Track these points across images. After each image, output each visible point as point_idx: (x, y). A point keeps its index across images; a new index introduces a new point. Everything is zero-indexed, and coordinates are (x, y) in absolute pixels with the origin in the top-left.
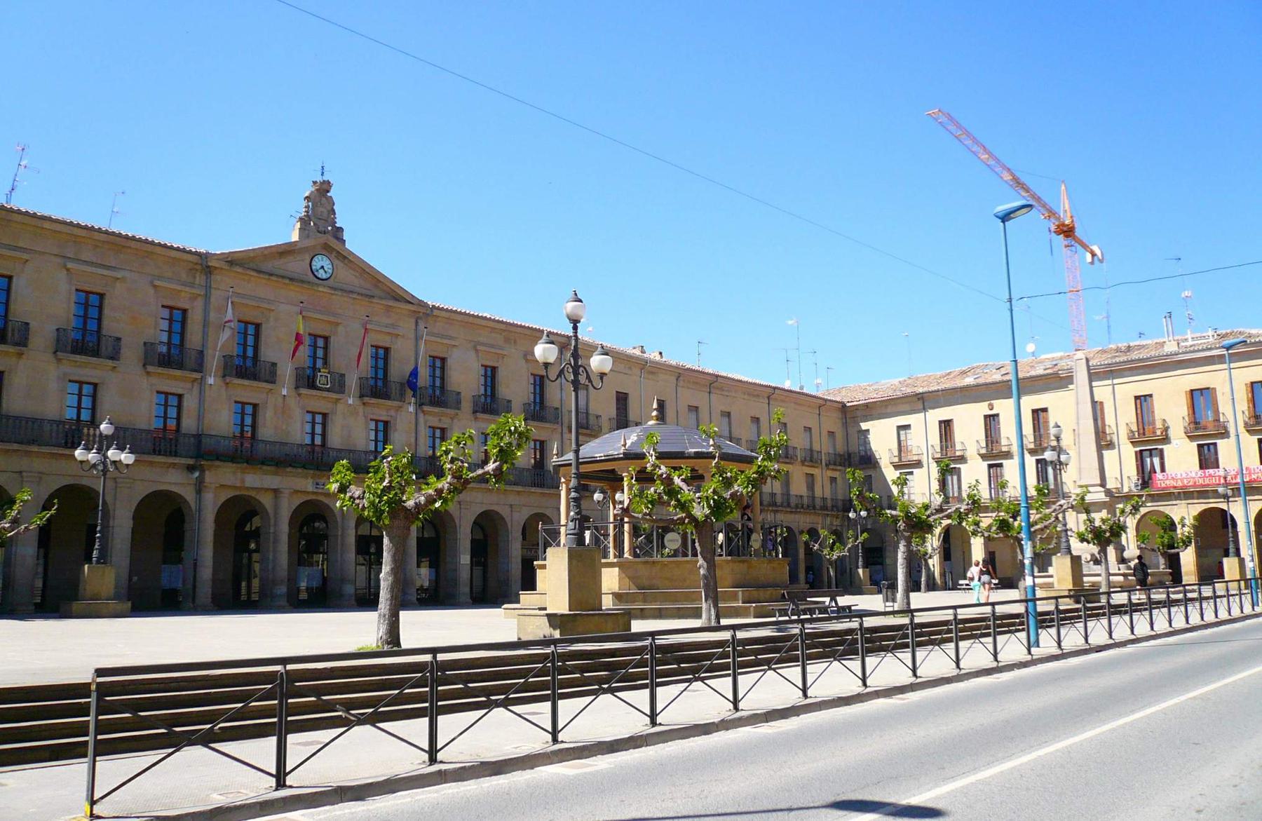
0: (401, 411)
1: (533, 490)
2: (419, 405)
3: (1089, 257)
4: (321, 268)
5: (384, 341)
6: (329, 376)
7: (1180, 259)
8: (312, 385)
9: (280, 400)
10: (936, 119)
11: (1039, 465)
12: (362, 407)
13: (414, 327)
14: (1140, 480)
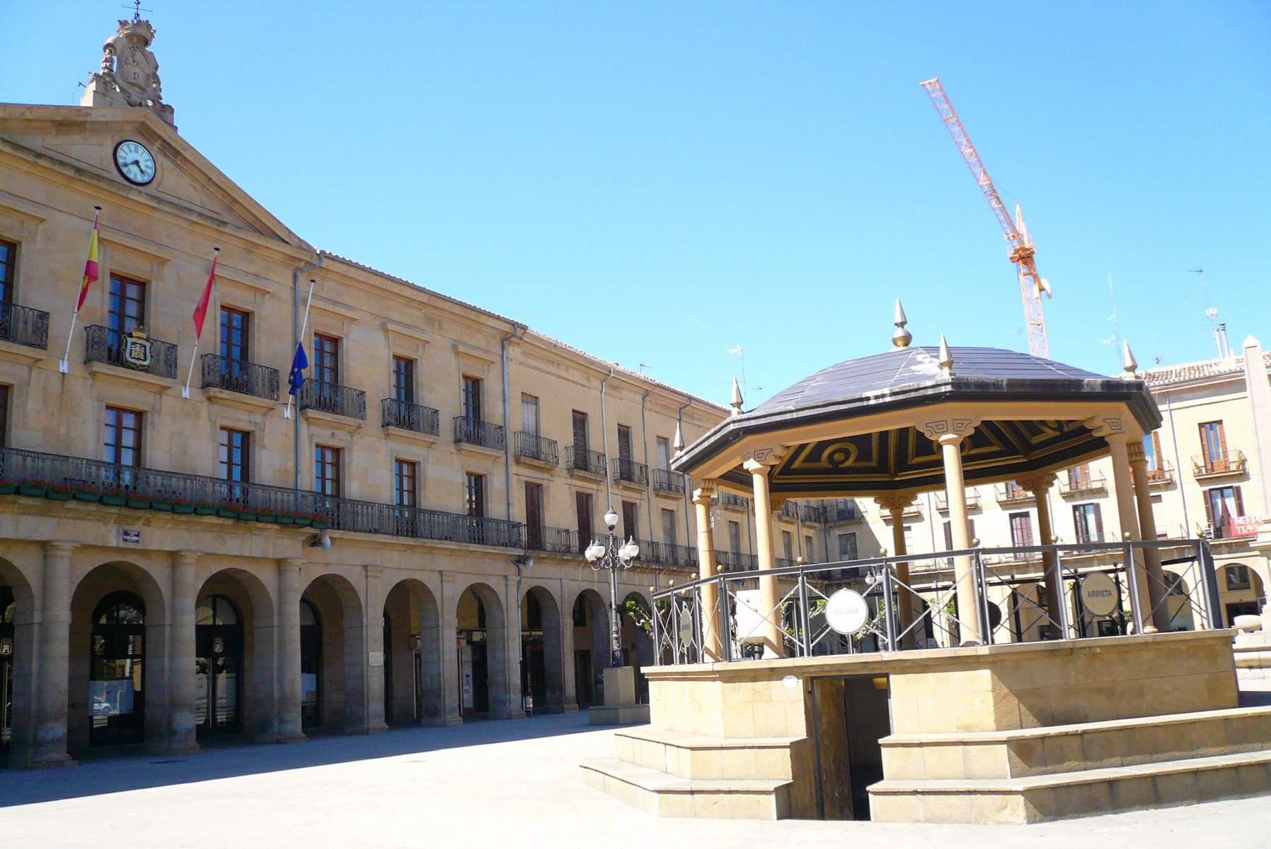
0: (272, 416)
1: (473, 547)
2: (301, 409)
3: (1036, 288)
4: (133, 163)
5: (242, 300)
6: (148, 345)
7: (1201, 271)
8: (116, 358)
9: (55, 381)
10: (929, 93)
11: (1077, 513)
12: (206, 404)
13: (290, 283)
14: (1212, 527)
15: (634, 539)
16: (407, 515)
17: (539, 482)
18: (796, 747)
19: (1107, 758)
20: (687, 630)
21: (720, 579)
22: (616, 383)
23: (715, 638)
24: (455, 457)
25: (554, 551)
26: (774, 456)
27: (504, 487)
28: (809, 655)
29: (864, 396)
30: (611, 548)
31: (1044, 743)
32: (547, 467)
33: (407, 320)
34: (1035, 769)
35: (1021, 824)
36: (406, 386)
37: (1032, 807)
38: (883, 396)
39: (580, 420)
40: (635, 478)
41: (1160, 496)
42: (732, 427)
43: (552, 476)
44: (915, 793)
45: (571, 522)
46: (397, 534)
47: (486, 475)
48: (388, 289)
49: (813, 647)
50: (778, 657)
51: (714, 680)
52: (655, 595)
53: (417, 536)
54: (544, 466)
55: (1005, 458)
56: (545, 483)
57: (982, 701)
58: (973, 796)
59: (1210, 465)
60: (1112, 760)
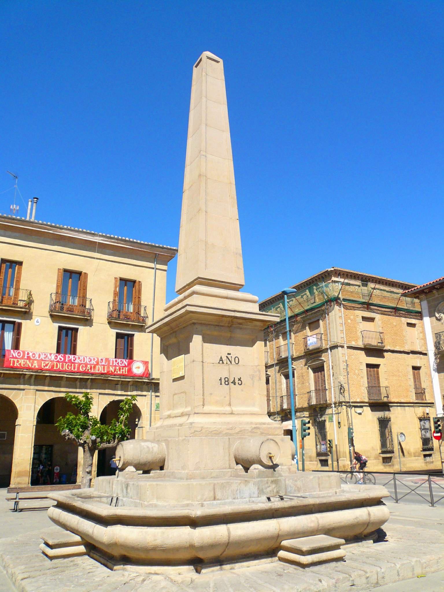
41: (133, 335)
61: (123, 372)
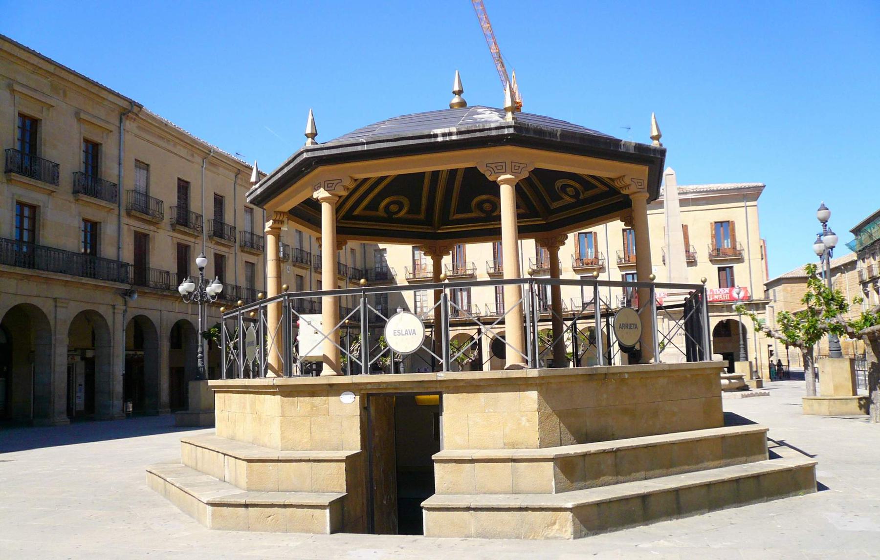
1: (85, 280)
7: (629, 128)
15: (219, 279)
16: (25, 249)
17: (147, 232)
18: (350, 461)
19: (634, 472)
20: (252, 347)
21: (284, 298)
22: (215, 161)
23: (278, 356)
24: (73, 206)
25: (155, 288)
26: (343, 186)
27: (116, 234)
28: (366, 373)
29: (432, 133)
30: (200, 285)
31: (584, 460)
32: (153, 220)
33: (32, 84)
34: (575, 484)
35: (568, 539)
36: (30, 141)
37: (579, 522)
38: (450, 134)
39: (183, 187)
40: (226, 236)
42: (305, 155)
43: (158, 228)
44: (468, 509)
45: (172, 266)
46: (15, 265)
47: (100, 223)
48: (16, 54)
49: (370, 365)
50: (335, 373)
51: (274, 394)
52: (224, 315)
53: (34, 268)
54: (151, 220)
55: (528, 220)
56: (151, 233)
57: (528, 421)
58: (525, 513)
59: (627, 257)
60: (638, 475)
61: (725, 298)
